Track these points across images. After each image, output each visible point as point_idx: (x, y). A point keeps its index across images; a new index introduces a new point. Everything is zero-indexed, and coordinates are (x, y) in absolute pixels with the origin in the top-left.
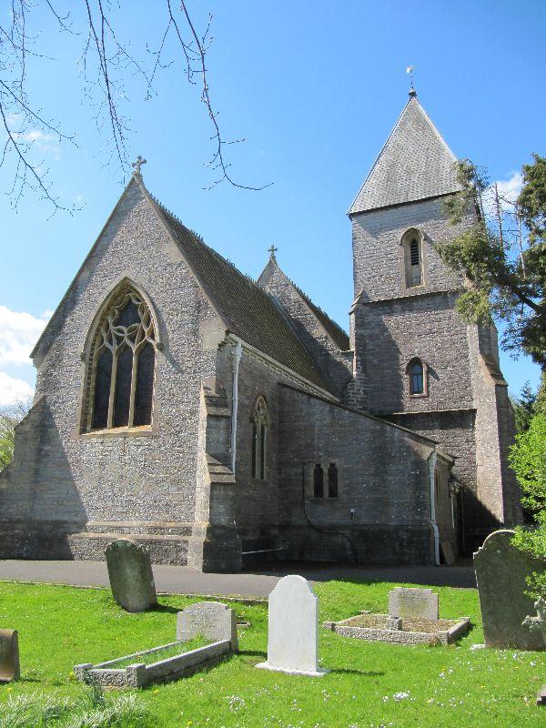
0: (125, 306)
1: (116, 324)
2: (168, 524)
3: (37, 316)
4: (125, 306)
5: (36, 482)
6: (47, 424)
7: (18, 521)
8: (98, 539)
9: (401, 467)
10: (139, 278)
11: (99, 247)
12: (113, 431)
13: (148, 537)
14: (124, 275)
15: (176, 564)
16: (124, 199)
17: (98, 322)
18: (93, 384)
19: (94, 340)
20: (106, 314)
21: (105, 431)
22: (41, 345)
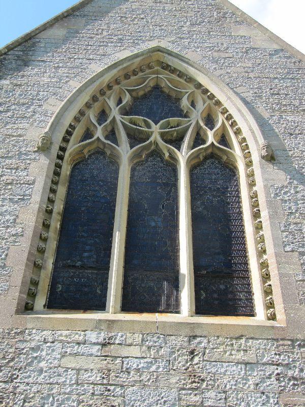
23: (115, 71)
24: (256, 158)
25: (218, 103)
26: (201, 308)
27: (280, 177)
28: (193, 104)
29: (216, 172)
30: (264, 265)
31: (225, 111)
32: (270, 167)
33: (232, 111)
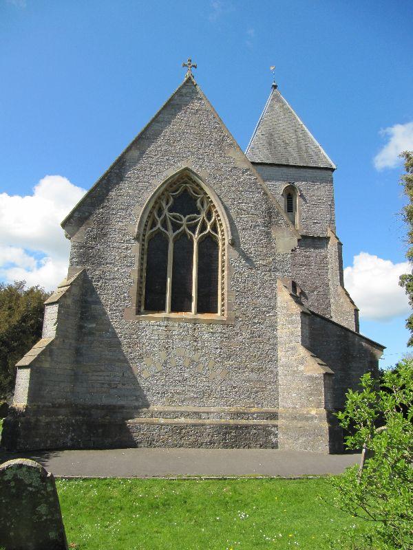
0: (183, 196)
1: (170, 210)
2: (253, 410)
3: (75, 182)
4: (183, 196)
5: (77, 362)
6: (90, 299)
7: (60, 406)
8: (171, 424)
9: (361, 365)
10: (202, 171)
11: (150, 132)
12: (174, 315)
13: (232, 422)
14: (182, 165)
15: (266, 447)
16: (179, 93)
17: (152, 204)
18: (145, 265)
19: (147, 222)
20: (159, 198)
21: (162, 315)
22: (76, 215)
23: (165, 185)
24: (226, 242)
25: (214, 206)
26: (200, 310)
27: (235, 254)
28: (202, 205)
29: (209, 244)
30: (223, 294)
31: (216, 212)
32: (231, 249)
33: (220, 213)
